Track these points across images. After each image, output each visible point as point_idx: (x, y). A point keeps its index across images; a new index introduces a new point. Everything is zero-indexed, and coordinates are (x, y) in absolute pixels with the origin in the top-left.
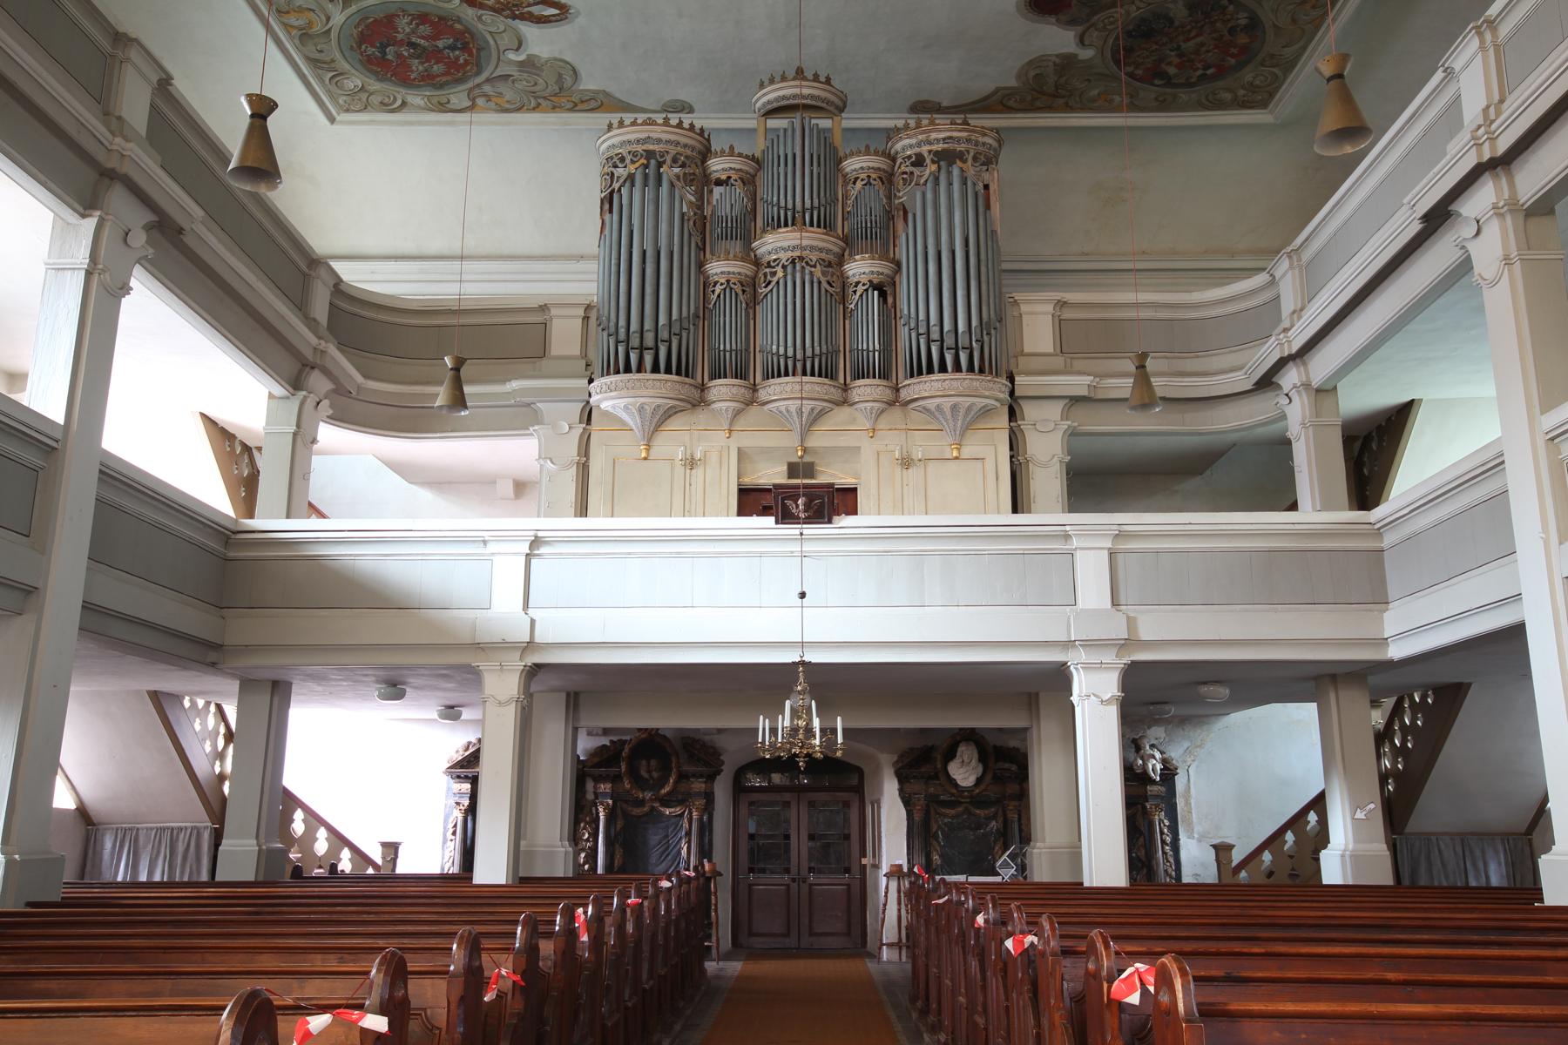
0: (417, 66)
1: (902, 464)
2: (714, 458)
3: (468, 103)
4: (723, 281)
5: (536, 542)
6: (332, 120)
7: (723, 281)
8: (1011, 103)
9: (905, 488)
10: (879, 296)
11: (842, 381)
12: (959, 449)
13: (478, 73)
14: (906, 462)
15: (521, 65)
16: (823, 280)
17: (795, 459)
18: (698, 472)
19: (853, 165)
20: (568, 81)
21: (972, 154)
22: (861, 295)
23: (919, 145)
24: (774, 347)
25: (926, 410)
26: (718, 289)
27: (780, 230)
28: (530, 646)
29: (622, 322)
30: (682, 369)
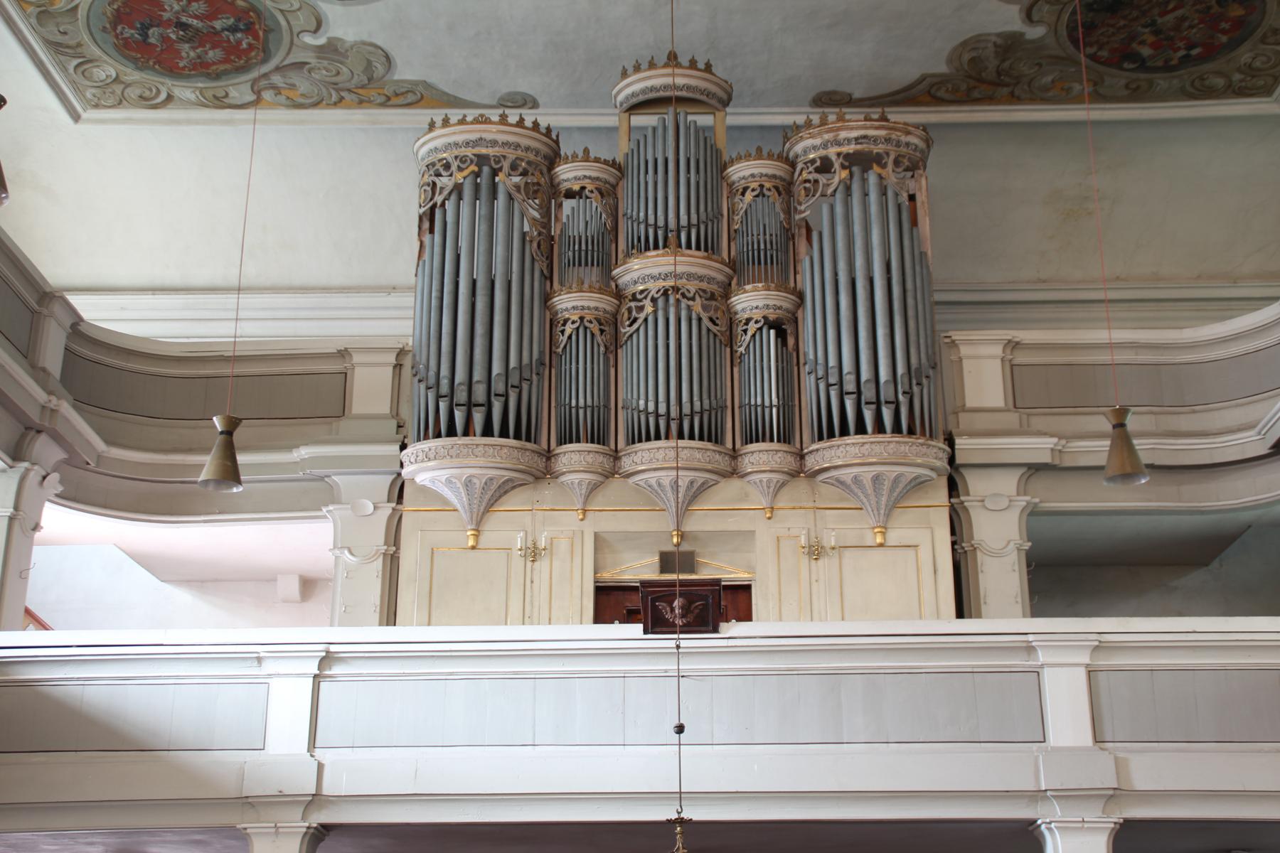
0: (187, 52)
1: (810, 553)
2: (563, 545)
3: (252, 97)
4: (575, 318)
5: (327, 659)
6: (76, 117)
7: (575, 318)
8: (941, 94)
9: (815, 585)
10: (777, 336)
11: (729, 445)
12: (884, 534)
13: (265, 61)
14: (815, 551)
15: (320, 49)
16: (704, 316)
17: (669, 548)
18: (543, 565)
19: (740, 171)
20: (379, 69)
21: (892, 157)
22: (754, 336)
23: (825, 145)
24: (642, 402)
25: (841, 483)
26: (569, 328)
27: (649, 254)
28: (316, 799)
29: (445, 371)
30: (523, 430)
